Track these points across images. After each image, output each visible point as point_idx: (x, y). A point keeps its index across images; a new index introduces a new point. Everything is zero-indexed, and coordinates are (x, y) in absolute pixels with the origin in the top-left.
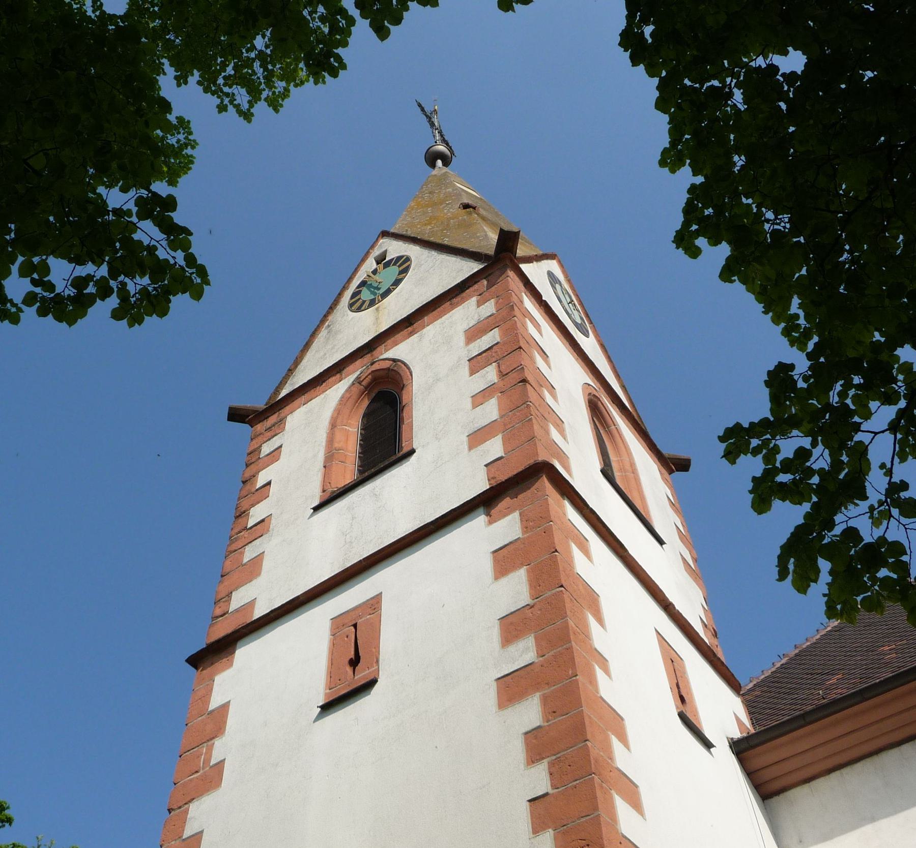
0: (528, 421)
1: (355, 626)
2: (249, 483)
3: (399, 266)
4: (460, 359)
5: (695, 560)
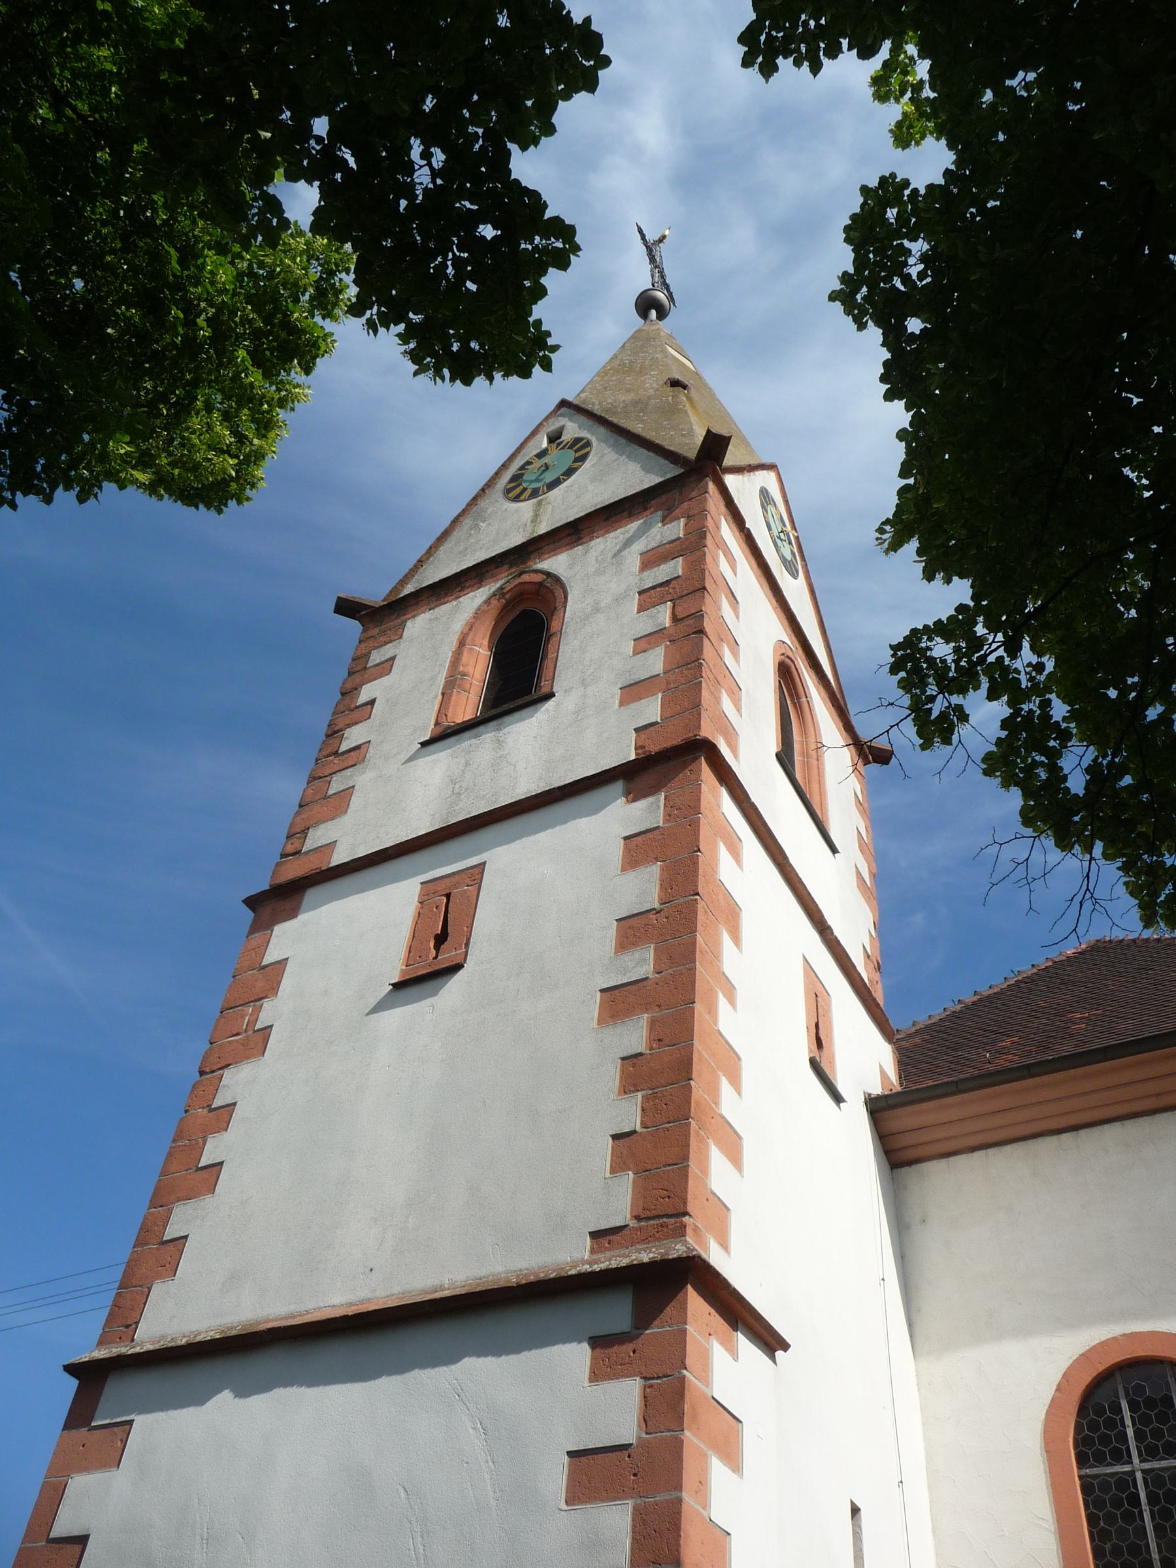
0: (696, 687)
1: (448, 896)
3: (576, 451)
5: (873, 876)
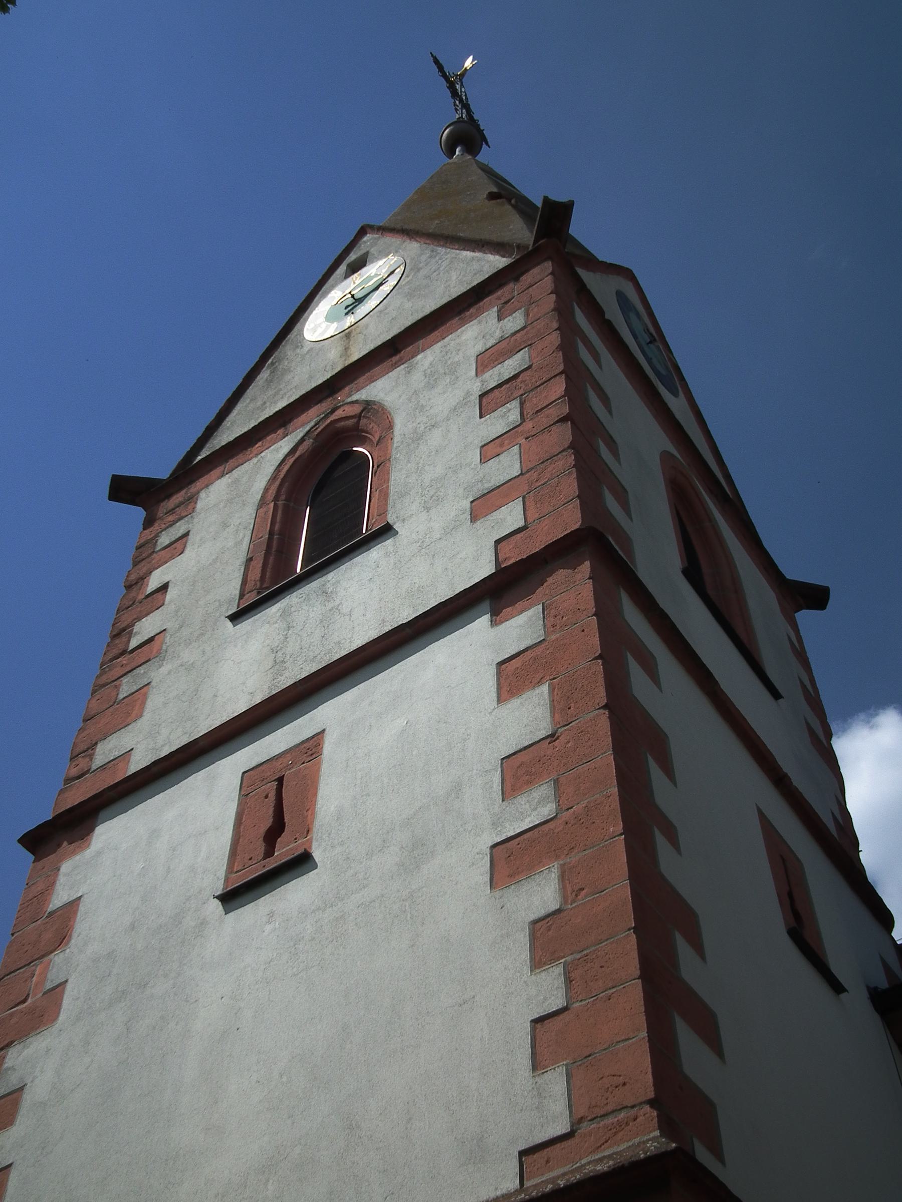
2: (135, 588)
4: (468, 393)
